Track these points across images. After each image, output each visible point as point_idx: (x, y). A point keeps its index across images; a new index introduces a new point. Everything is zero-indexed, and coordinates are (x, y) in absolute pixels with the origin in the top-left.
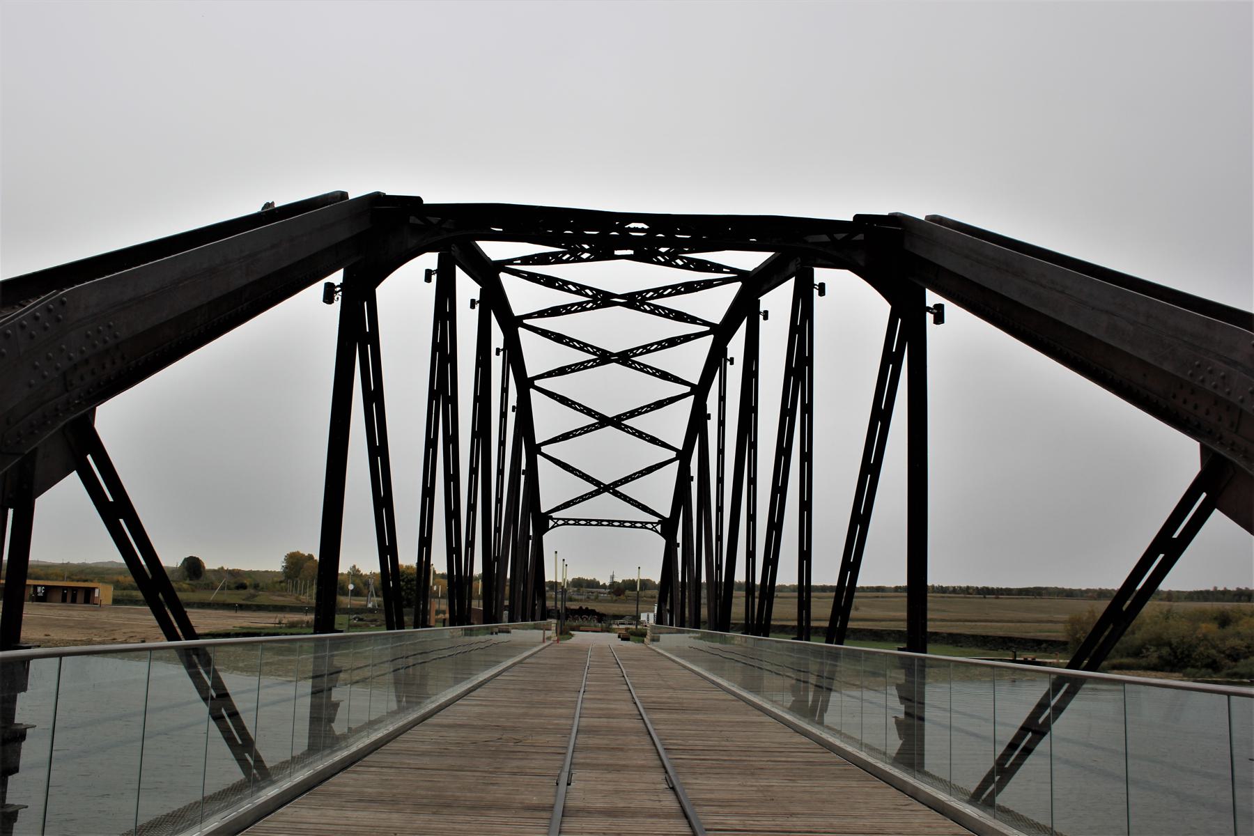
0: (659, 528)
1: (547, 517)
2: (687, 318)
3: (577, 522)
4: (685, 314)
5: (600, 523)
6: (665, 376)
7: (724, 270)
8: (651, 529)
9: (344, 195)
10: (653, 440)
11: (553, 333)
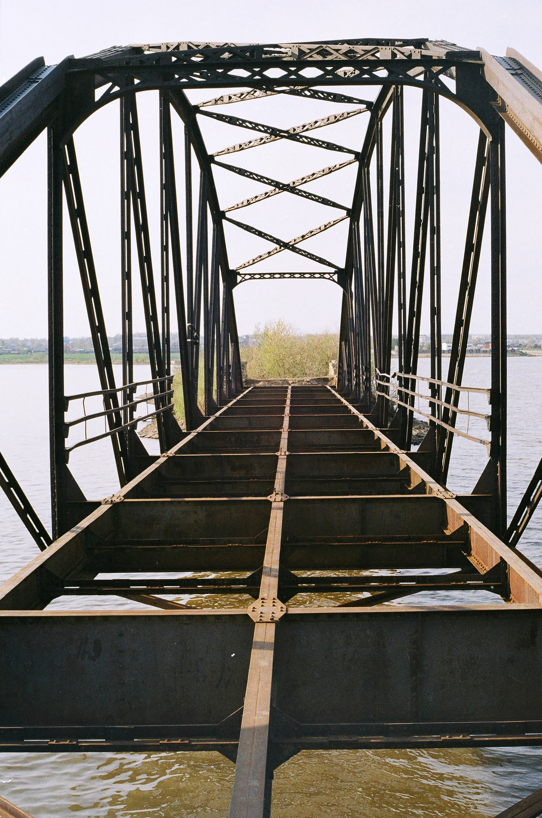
0: (335, 277)
1: (235, 273)
3: (262, 276)
4: (342, 95)
5: (282, 275)
6: (330, 146)
7: (354, 101)
8: (329, 279)
10: (325, 202)
11: (227, 117)
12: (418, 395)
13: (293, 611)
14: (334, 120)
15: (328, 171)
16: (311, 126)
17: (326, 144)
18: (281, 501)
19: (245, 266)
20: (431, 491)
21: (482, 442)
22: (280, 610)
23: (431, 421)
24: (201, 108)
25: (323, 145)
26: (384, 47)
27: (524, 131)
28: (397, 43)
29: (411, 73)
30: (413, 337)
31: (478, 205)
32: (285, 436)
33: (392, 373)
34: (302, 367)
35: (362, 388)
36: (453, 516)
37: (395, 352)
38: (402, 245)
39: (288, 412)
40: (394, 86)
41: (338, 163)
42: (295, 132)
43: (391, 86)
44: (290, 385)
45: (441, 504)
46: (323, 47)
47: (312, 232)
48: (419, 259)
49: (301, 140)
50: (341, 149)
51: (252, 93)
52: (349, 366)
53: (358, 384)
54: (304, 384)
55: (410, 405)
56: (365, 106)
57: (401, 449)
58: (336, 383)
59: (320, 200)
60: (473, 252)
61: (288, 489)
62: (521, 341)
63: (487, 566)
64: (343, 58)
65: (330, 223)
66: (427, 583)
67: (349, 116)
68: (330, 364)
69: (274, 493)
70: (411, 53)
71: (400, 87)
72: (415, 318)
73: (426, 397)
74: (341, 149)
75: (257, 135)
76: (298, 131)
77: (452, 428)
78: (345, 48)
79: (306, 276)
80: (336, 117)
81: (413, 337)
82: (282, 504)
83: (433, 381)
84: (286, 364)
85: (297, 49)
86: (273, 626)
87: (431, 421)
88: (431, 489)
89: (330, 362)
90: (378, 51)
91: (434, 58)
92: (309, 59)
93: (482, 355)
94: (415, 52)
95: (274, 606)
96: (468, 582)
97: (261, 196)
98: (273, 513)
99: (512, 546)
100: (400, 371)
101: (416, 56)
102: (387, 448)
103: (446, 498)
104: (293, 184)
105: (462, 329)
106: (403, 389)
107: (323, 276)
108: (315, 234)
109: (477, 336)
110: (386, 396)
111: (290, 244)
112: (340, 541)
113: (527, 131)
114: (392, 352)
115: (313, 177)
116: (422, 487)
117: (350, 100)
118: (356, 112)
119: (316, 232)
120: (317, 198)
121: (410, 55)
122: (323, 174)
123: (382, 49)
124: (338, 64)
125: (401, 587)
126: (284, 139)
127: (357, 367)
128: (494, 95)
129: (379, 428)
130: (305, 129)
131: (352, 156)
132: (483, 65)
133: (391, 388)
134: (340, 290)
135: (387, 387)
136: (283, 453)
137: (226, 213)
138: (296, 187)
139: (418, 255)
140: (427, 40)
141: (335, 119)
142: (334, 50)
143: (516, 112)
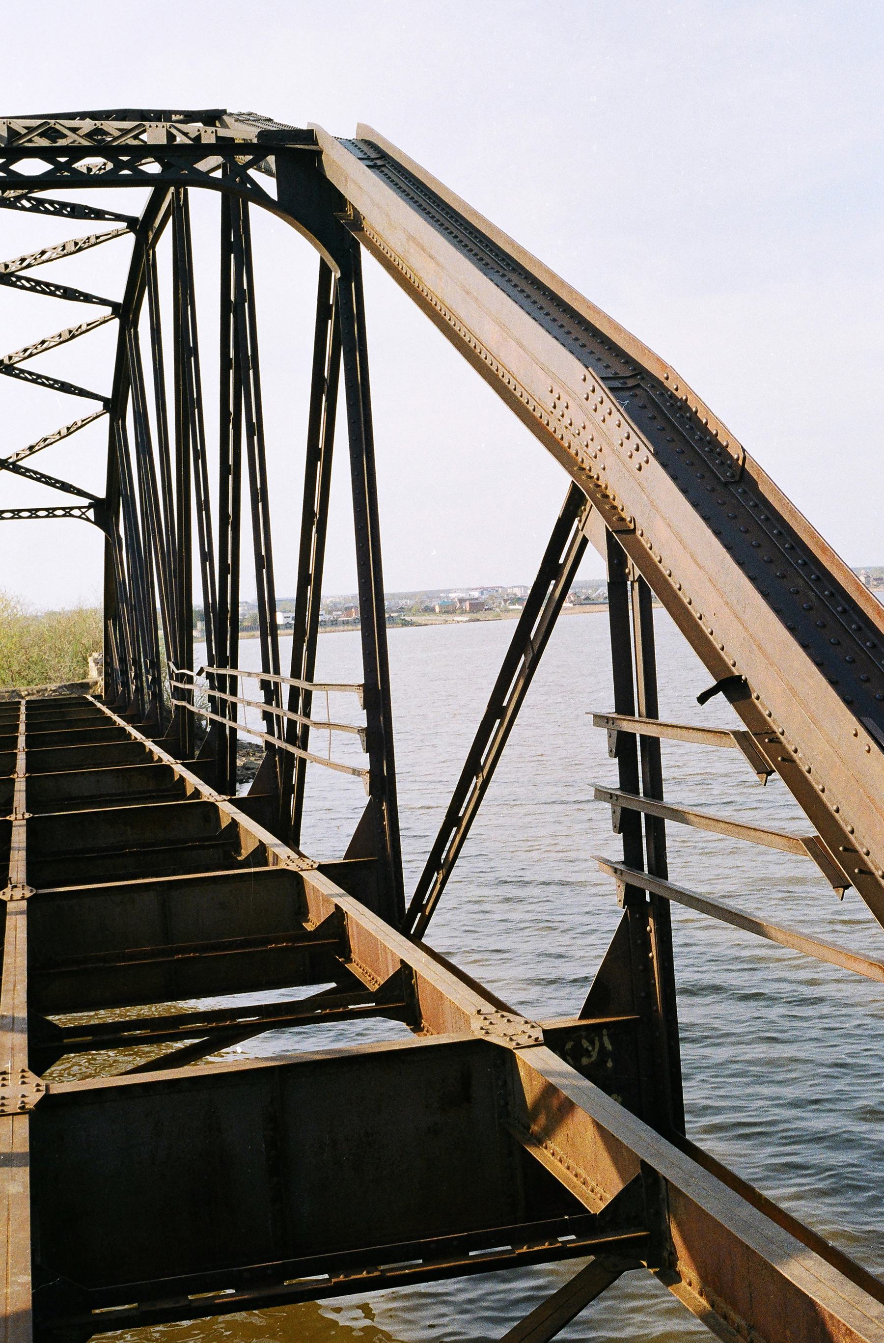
0: (91, 514)
4: (86, 207)
6: (70, 294)
7: (107, 216)
8: (80, 517)
10: (66, 388)
12: (242, 701)
13: (58, 1088)
14: (73, 249)
15: (67, 336)
16: (35, 259)
17: (62, 291)
18: (23, 898)
20: (277, 860)
21: (356, 772)
22: (35, 1090)
23: (267, 742)
25: (58, 293)
26: (154, 124)
27: (392, 259)
28: (174, 118)
29: (203, 166)
30: (229, 606)
31: (324, 385)
32: (20, 786)
33: (196, 669)
34: (43, 667)
35: (148, 696)
36: (317, 897)
37: (199, 631)
38: (201, 454)
39: (24, 745)
40: (172, 189)
41: (84, 321)
42: (8, 271)
43: (168, 190)
44: (23, 698)
45: (295, 880)
46: (49, 124)
47: (45, 440)
48: (231, 477)
49: (18, 283)
50: (87, 298)
52: (123, 660)
53: (140, 690)
54: (48, 696)
55: (230, 719)
56: (125, 224)
57: (220, 793)
58: (102, 689)
59: (56, 386)
60: (320, 461)
61: (32, 880)
62: (402, 603)
63: (379, 976)
64: (85, 143)
65: (75, 423)
66: (282, 1016)
67: (98, 241)
68: (90, 660)
69: (10, 886)
70: (200, 134)
71: (182, 190)
72: (229, 576)
73: (257, 705)
74: (87, 298)
75: (35, 273)
76: (12, 268)
77: (303, 752)
78: (88, 125)
79: (41, 513)
80: (76, 244)
81: (229, 606)
82: (24, 904)
83: (266, 677)
84: (15, 663)
85: (5, 127)
86: (24, 1121)
87: (267, 742)
88: (276, 857)
89: (90, 656)
90: (144, 131)
91: (236, 141)
92: (26, 144)
93: (341, 628)
94: (206, 132)
95: (23, 1083)
96: (351, 1007)
98: (10, 922)
99: (416, 938)
100: (211, 664)
101: (209, 138)
102: (197, 793)
103: (302, 870)
105: (310, 590)
106: (217, 694)
107: (68, 512)
108: (51, 444)
109: (331, 599)
110: (189, 706)
111: (10, 461)
112: (132, 957)
113: (397, 259)
114: (195, 633)
115: (43, 346)
116: (261, 854)
117: (99, 215)
118: (110, 234)
119: (53, 440)
120: (51, 382)
121: (199, 137)
122: (59, 341)
123: (150, 126)
124: (78, 153)
125: (239, 1025)
127: (137, 662)
128: (340, 201)
129: (180, 760)
130: (25, 264)
131: (108, 310)
132: (320, 153)
133: (197, 693)
134: (100, 535)
135: (190, 691)
136: (20, 817)
138: (15, 365)
139: (230, 470)
140: (224, 112)
141: (75, 246)
142: (70, 129)
143: (378, 229)
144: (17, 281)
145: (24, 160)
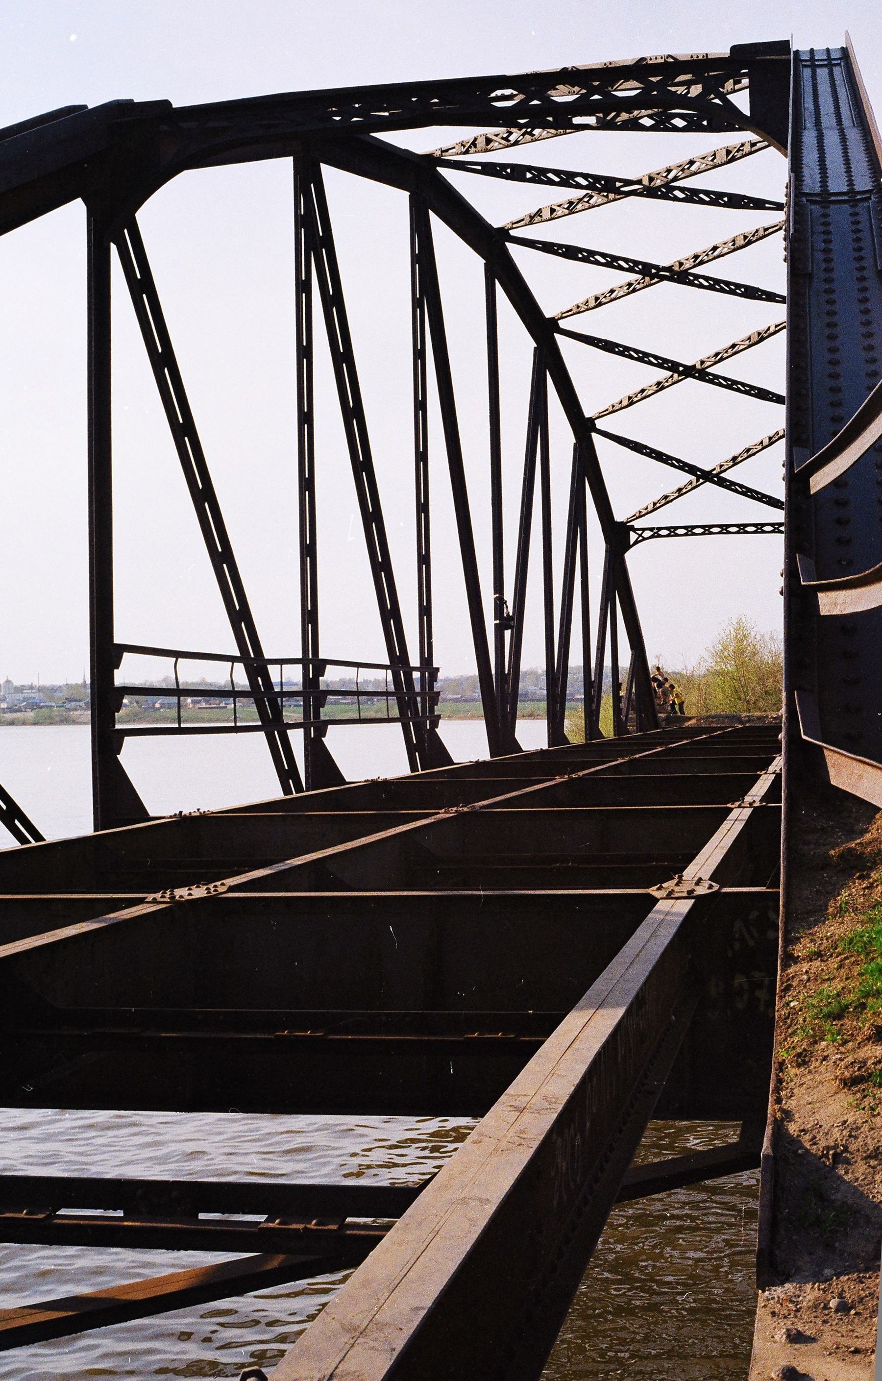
2: (749, 203)
3: (672, 531)
4: (745, 197)
5: (707, 530)
7: (479, 168)
9: (85, 107)
14: (743, 243)
16: (707, 255)
19: (641, 514)
24: (513, 233)
47: (748, 450)
51: (586, 199)
65: (777, 433)
75: (620, 278)
79: (697, 531)
80: (745, 237)
97: (650, 388)
104: (701, 365)
107: (778, 528)
111: (714, 472)
115: (734, 349)
117: (540, 176)
118: (777, 225)
119: (755, 450)
126: (665, 282)
137: (596, 421)
138: (708, 370)
144: (695, 279)
145: (85, 208)
